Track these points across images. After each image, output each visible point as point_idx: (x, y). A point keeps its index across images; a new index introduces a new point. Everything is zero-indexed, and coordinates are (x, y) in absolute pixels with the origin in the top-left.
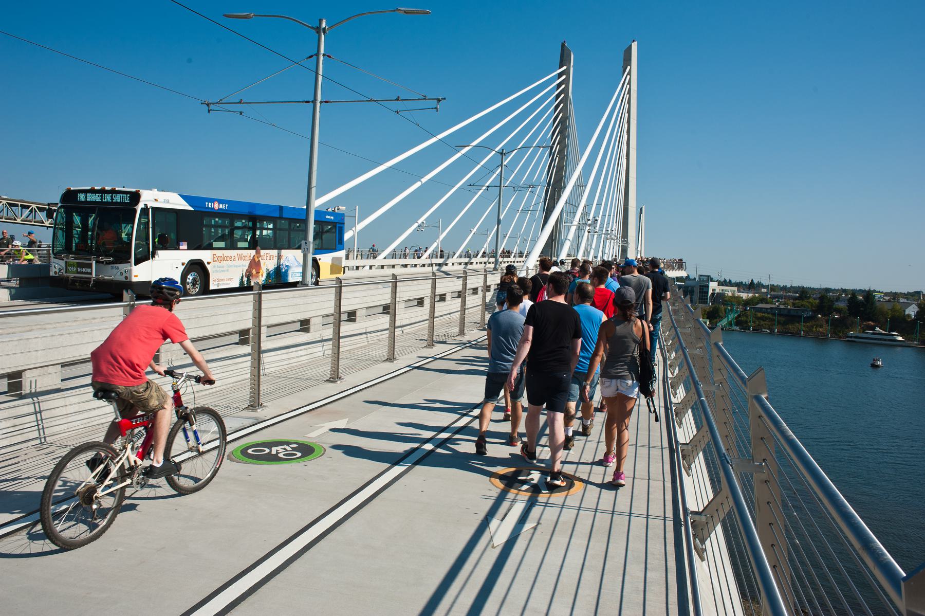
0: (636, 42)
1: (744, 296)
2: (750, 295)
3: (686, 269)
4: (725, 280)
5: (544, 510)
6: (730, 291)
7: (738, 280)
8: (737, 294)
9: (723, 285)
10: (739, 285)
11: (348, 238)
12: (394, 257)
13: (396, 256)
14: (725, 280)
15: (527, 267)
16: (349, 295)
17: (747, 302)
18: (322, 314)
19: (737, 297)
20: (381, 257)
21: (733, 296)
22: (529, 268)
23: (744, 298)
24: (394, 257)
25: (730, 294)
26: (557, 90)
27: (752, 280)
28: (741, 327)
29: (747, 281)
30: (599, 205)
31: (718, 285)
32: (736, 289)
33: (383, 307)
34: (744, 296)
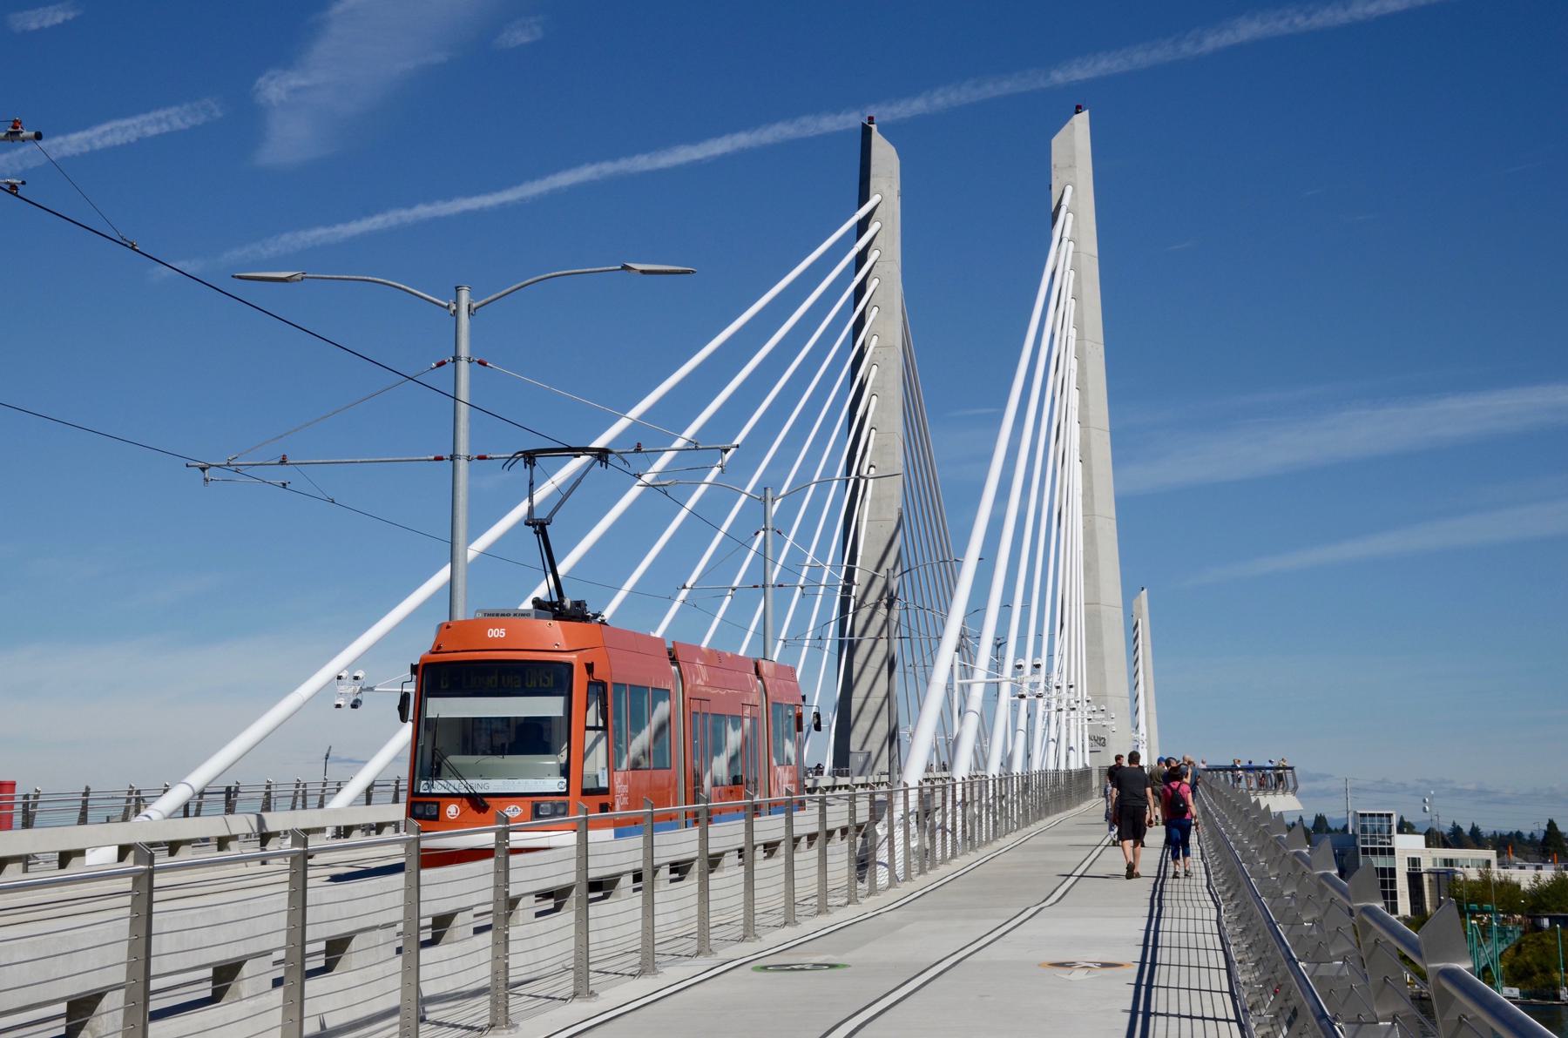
0: (1085, 115)
1: (1525, 877)
2: (1548, 873)
3: (1296, 788)
4: (1457, 830)
5: (911, 575)
6: (1471, 863)
7: (1506, 827)
8: (1497, 873)
9: (1446, 845)
10: (1508, 845)
11: (1300, 805)
12: (300, 801)
13: (304, 801)
14: (1457, 830)
15: (906, 785)
16: (263, 925)
17: (1540, 900)
18: (325, 936)
19: (1501, 884)
20: (339, 802)
21: (1486, 882)
22: (910, 786)
23: (1525, 886)
24: (300, 801)
25: (1473, 875)
26: (859, 238)
27: (1551, 824)
28: (1528, 989)
29: (1532, 825)
30: (1006, 606)
31: (1428, 845)
32: (1491, 854)
33: (634, 876)
34: (1525, 877)
